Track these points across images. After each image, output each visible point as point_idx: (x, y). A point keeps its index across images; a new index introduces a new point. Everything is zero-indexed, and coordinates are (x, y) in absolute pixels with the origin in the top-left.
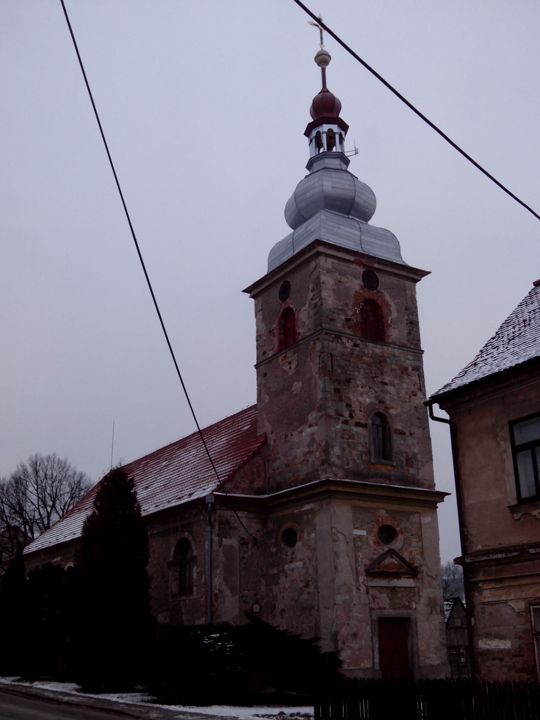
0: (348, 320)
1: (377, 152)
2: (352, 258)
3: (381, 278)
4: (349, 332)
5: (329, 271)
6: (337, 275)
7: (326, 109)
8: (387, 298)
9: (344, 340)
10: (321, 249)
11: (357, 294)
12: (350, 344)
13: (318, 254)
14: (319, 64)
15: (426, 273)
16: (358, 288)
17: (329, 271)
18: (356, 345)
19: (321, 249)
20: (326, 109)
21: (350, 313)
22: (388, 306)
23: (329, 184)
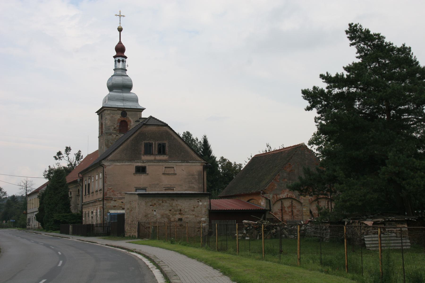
0: (114, 128)
1: (136, 70)
2: (116, 109)
3: (128, 113)
4: (115, 132)
5: (109, 114)
6: (112, 115)
7: (120, 50)
8: (130, 119)
9: (113, 135)
10: (105, 108)
11: (119, 119)
12: (115, 136)
13: (105, 110)
14: (119, 30)
15: (143, 109)
16: (119, 117)
17: (109, 114)
18: (117, 136)
19: (105, 108)
20: (120, 50)
21: (116, 126)
22: (130, 121)
23: (119, 80)
